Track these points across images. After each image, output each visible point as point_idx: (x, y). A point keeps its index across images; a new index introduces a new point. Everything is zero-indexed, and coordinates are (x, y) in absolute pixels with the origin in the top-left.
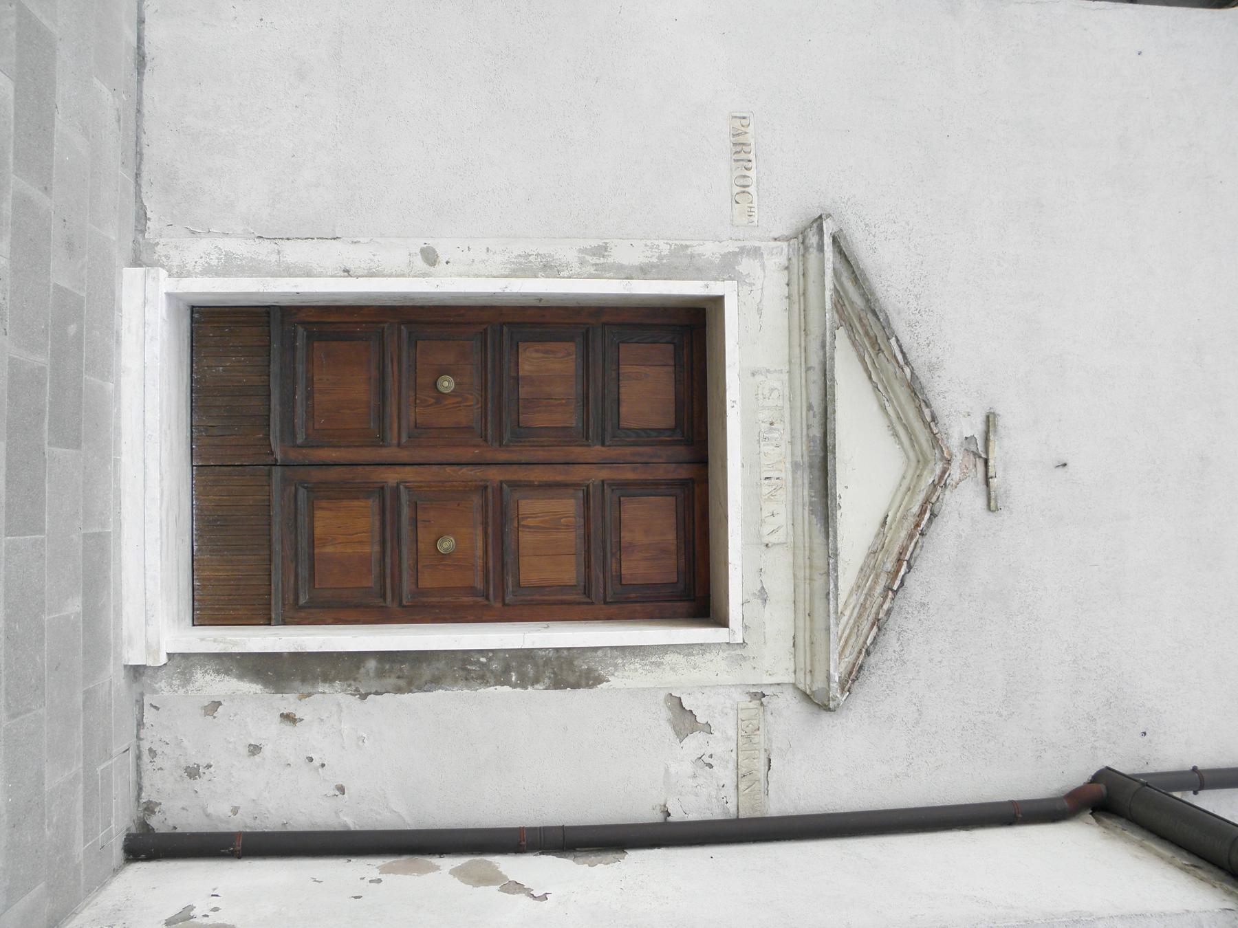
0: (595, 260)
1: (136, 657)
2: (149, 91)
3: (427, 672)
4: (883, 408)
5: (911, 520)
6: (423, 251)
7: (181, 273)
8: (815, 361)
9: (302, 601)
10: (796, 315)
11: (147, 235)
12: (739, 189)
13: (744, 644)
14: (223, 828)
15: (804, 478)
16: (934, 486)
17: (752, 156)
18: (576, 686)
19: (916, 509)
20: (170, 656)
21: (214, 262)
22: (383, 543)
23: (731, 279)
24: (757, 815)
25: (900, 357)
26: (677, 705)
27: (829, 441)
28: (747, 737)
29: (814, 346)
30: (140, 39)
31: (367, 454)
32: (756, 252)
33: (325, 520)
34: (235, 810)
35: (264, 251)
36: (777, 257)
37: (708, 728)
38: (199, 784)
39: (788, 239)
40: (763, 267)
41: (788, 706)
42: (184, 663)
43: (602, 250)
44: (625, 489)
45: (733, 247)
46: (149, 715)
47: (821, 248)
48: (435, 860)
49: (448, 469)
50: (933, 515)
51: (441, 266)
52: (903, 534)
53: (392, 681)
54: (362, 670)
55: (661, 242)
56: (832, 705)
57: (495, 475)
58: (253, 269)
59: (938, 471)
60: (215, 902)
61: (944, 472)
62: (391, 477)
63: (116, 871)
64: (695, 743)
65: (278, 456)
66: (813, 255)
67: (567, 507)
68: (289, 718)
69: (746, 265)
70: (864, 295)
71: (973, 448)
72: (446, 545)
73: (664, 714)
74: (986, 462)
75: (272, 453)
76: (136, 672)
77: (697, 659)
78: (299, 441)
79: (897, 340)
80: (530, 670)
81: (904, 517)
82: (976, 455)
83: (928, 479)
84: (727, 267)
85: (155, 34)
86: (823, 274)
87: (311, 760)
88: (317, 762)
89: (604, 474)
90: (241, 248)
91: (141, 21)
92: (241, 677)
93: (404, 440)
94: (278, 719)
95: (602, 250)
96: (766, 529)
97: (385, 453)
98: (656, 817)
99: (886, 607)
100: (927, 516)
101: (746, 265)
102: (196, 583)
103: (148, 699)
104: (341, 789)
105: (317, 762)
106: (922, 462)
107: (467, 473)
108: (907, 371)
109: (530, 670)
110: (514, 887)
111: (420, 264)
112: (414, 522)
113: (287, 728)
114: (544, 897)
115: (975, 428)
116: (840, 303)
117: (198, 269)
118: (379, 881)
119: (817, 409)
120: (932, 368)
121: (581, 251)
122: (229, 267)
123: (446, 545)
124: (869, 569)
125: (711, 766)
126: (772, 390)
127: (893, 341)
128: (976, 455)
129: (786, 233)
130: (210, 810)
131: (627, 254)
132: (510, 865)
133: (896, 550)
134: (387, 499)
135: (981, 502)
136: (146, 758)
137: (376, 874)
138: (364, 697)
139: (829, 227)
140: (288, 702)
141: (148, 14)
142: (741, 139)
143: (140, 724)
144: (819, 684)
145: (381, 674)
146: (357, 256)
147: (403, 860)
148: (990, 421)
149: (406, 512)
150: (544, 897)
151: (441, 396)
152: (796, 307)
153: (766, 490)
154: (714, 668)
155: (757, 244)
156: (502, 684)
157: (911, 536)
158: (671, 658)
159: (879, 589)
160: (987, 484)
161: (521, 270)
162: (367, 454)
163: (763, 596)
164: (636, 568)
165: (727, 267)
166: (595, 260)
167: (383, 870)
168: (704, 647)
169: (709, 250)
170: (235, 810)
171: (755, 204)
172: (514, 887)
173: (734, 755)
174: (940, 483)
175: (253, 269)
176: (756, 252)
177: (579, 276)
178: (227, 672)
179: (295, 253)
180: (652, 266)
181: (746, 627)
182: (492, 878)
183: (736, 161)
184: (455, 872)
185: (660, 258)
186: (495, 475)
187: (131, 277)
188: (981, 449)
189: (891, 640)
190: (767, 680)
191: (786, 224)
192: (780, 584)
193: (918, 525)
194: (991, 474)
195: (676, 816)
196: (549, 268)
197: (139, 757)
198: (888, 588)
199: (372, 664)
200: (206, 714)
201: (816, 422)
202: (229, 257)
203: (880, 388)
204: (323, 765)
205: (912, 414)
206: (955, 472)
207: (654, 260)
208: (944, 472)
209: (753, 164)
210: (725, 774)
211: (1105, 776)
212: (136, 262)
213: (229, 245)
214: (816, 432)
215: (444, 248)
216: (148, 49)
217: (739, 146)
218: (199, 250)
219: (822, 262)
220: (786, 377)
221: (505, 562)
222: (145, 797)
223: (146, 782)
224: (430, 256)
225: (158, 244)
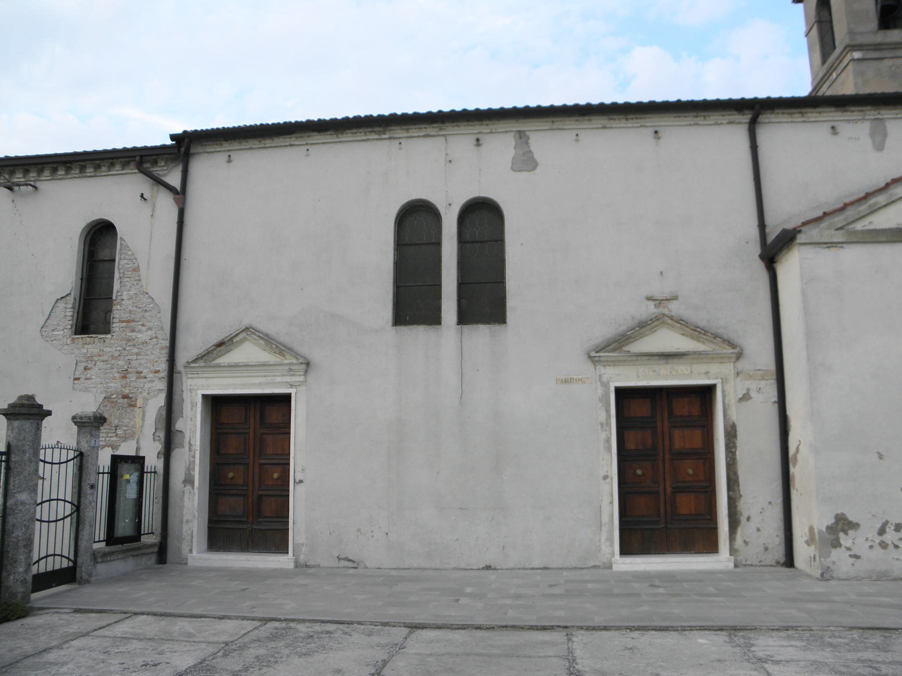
0: (605, 426)
1: (731, 565)
2: (555, 566)
3: (732, 476)
4: (647, 335)
5: (682, 327)
6: (604, 479)
7: (613, 554)
8: (635, 358)
9: (709, 517)
10: (402, 213)
11: (600, 565)
12: (580, 382)
13: (722, 379)
14: (783, 540)
15: (671, 361)
16: (671, 319)
17: (569, 377)
18: (736, 431)
19: (679, 325)
20: (731, 555)
21: (608, 544)
22: (690, 492)
23: (609, 384)
24: (775, 373)
25: (632, 331)
26: (741, 400)
27: (659, 354)
28: (750, 377)
29: (630, 358)
30: (538, 569)
31: (662, 498)
32: (600, 376)
33: (683, 511)
34: (778, 536)
35: (605, 528)
36: (601, 370)
37: (748, 390)
38: (770, 547)
39: (595, 366)
40: (605, 374)
41: (742, 365)
42: (733, 551)
43: (602, 424)
44: (671, 414)
45: (599, 383)
46: (749, 563)
47: (599, 357)
48: (791, 473)
49: (666, 471)
50: (681, 320)
51: (609, 474)
52: (687, 329)
53: (736, 487)
54: (733, 496)
55: (599, 406)
56: (740, 352)
57: (667, 457)
58: (611, 531)
59: (666, 318)
60: (804, 535)
61: (667, 316)
62: (669, 489)
63: (797, 569)
64: (753, 394)
65: (663, 526)
66: (602, 359)
67: (677, 433)
68: (748, 519)
69: (605, 379)
70: (614, 343)
71: (658, 305)
72: (690, 472)
73: (744, 403)
74: (662, 300)
75: (662, 528)
76: (736, 566)
77: (727, 393)
78: (658, 519)
79: (627, 332)
80: (731, 445)
81: (682, 329)
82: (660, 303)
83: (670, 321)
84: (605, 385)
85: (536, 564)
86: (608, 356)
87: (761, 512)
88: (762, 510)
89: (666, 421)
90: (604, 536)
91: (533, 569)
92: (736, 534)
93: (657, 485)
94: (749, 522)
95: (602, 424)
96: (686, 373)
97: (661, 492)
98: (776, 405)
99: (710, 335)
100: (681, 322)
101: (605, 379)
102: (705, 552)
103: (744, 563)
104: (770, 503)
105: (762, 510)
106: (664, 323)
107: (667, 465)
108: (637, 329)
109: (731, 445)
110: (797, 450)
111: (608, 480)
112: (683, 482)
113: (751, 519)
114: (800, 441)
115: (651, 305)
116: (614, 350)
117: (611, 549)
118: (797, 489)
119: (650, 357)
120: (633, 318)
121: (602, 431)
122: (610, 540)
123: (690, 472)
124: (698, 339)
125: (760, 389)
126: (643, 371)
127: (628, 333)
128: (660, 303)
129: (593, 366)
130: (778, 543)
131: (602, 417)
132: (792, 451)
133: (691, 331)
134: (677, 490)
135: (675, 302)
136: (762, 564)
137: (795, 490)
138: (741, 496)
139: (593, 354)
140: (743, 519)
141: (530, 567)
142: (564, 381)
143: (751, 565)
144: (734, 356)
145: (734, 491)
146: (606, 500)
147: (791, 483)
148: (649, 299)
149: (680, 485)
150: (800, 441)
151: (643, 474)
152: (617, 364)
153: (674, 373)
154: (729, 388)
155: (598, 376)
156: (735, 453)
157: (688, 327)
158: (726, 401)
159: (705, 337)
160: (669, 300)
161: (609, 449)
162: (662, 498)
163: (707, 373)
164: (696, 410)
165: (605, 385)
166: (605, 426)
167: (794, 489)
168: (723, 391)
169: (600, 391)
170: (778, 536)
171: (585, 376)
172: (797, 450)
173: (756, 381)
174: (671, 318)
175: (611, 531)
176: (600, 376)
177: (611, 431)
178: (735, 538)
179: (605, 519)
180: (606, 409)
181: (717, 378)
182: (795, 456)
183: (571, 382)
184: (794, 466)
185: (603, 406)
186: (667, 457)
187: (616, 568)
188: (658, 302)
189: (720, 331)
190: (733, 372)
191: (589, 367)
192: (703, 368)
193: (684, 325)
194: (665, 298)
195: (776, 399)
196: (608, 440)
197: (762, 566)
198: (704, 334)
199: (731, 493)
200: (748, 544)
201: (654, 358)
202: (607, 539)
203: (642, 336)
204: (763, 508)
205: (649, 327)
206: (666, 311)
207: (604, 408)
208: (667, 316)
209: (572, 377)
210: (763, 384)
211: (762, 257)
212: (610, 567)
213: (603, 540)
214: (656, 358)
215: (603, 473)
216: (542, 566)
217: (566, 381)
218: (605, 549)
219: (604, 356)
220: (639, 367)
221: (235, 364)
222: (774, 564)
223: (770, 564)
224: (606, 477)
225: (603, 562)
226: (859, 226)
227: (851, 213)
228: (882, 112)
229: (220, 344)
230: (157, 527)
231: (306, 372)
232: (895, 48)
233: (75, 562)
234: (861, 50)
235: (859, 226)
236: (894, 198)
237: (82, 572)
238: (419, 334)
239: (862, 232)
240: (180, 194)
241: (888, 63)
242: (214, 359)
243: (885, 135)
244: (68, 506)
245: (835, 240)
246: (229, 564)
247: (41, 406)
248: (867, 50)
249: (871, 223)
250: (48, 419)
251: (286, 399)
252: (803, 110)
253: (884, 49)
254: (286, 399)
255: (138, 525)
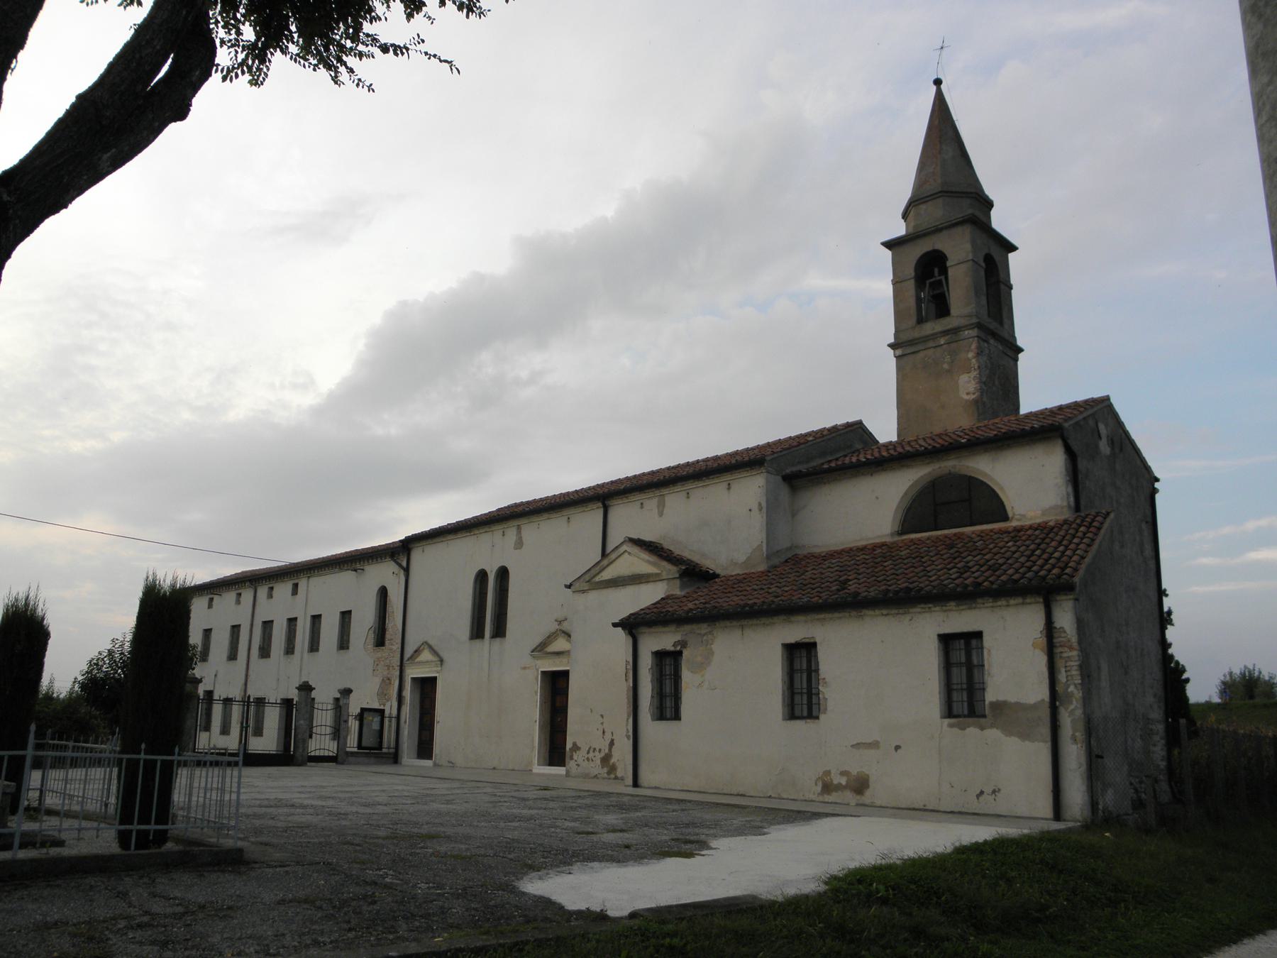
182: (629, 716)
226: (597, 579)
227: (593, 572)
228: (662, 490)
229: (416, 651)
230: (393, 744)
231: (442, 665)
232: (925, 341)
233: (337, 754)
234: (901, 347)
235: (597, 579)
236: (611, 561)
237: (339, 759)
238: (477, 643)
239: (598, 582)
240: (407, 571)
241: (921, 355)
242: (415, 659)
243: (664, 506)
244: (328, 728)
245: (585, 589)
246: (425, 765)
247: (311, 686)
248: (906, 346)
249: (602, 577)
250: (314, 691)
251: (435, 678)
252: (626, 495)
253: (916, 344)
254: (435, 678)
255: (381, 742)
